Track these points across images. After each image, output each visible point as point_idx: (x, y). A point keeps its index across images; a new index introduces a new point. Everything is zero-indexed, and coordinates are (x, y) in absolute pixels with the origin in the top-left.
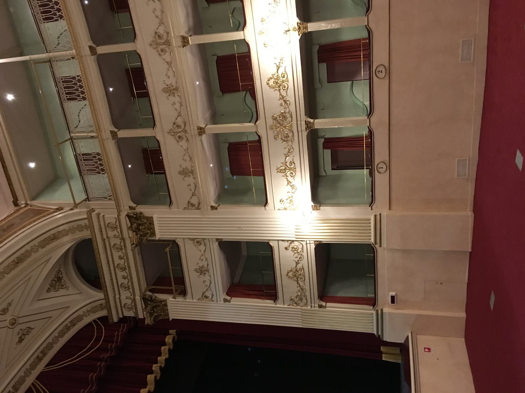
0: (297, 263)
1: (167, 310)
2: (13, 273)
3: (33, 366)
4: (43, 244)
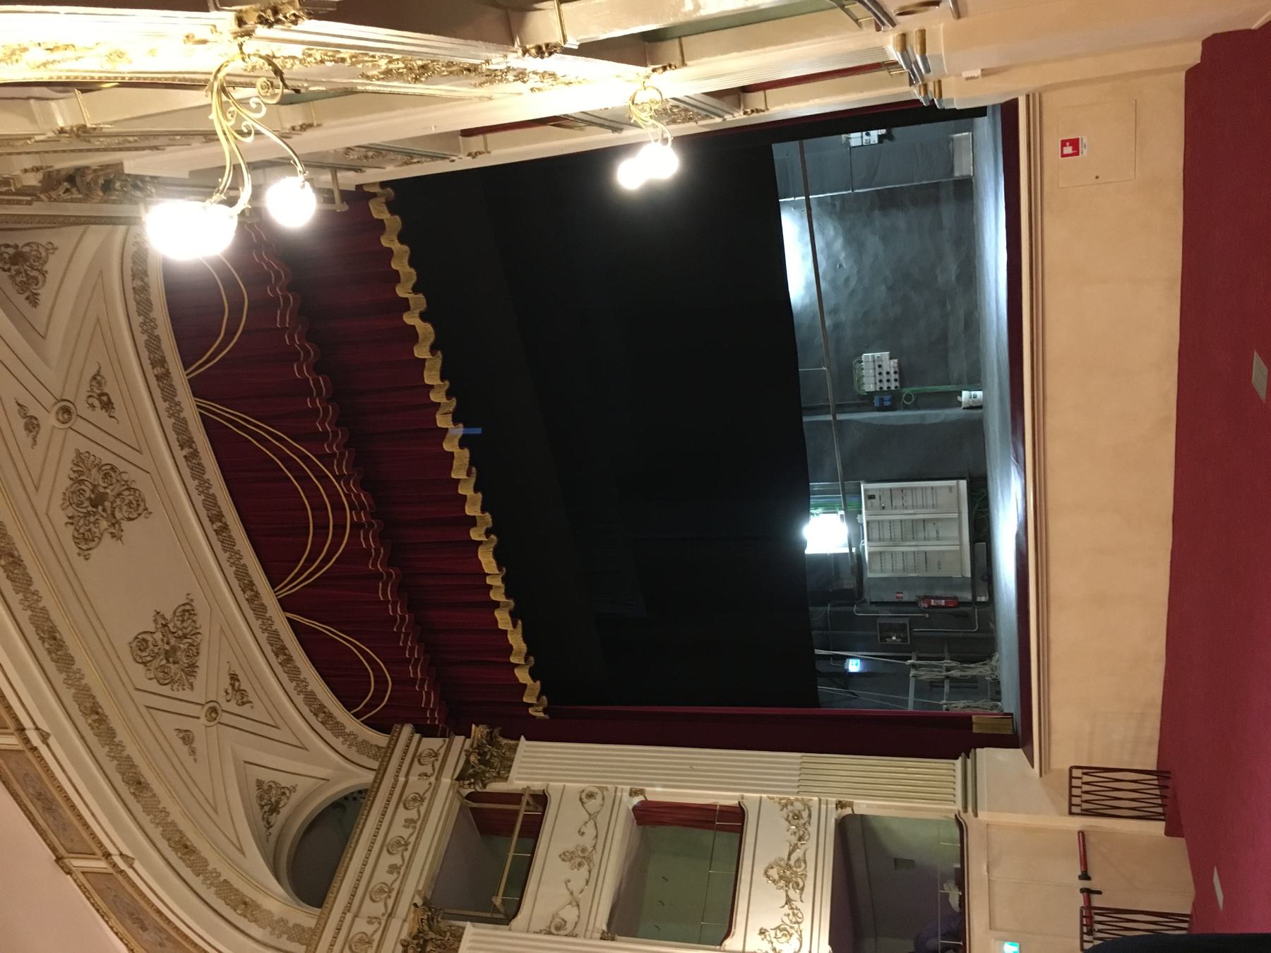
1: (512, 760)
3: (169, 393)
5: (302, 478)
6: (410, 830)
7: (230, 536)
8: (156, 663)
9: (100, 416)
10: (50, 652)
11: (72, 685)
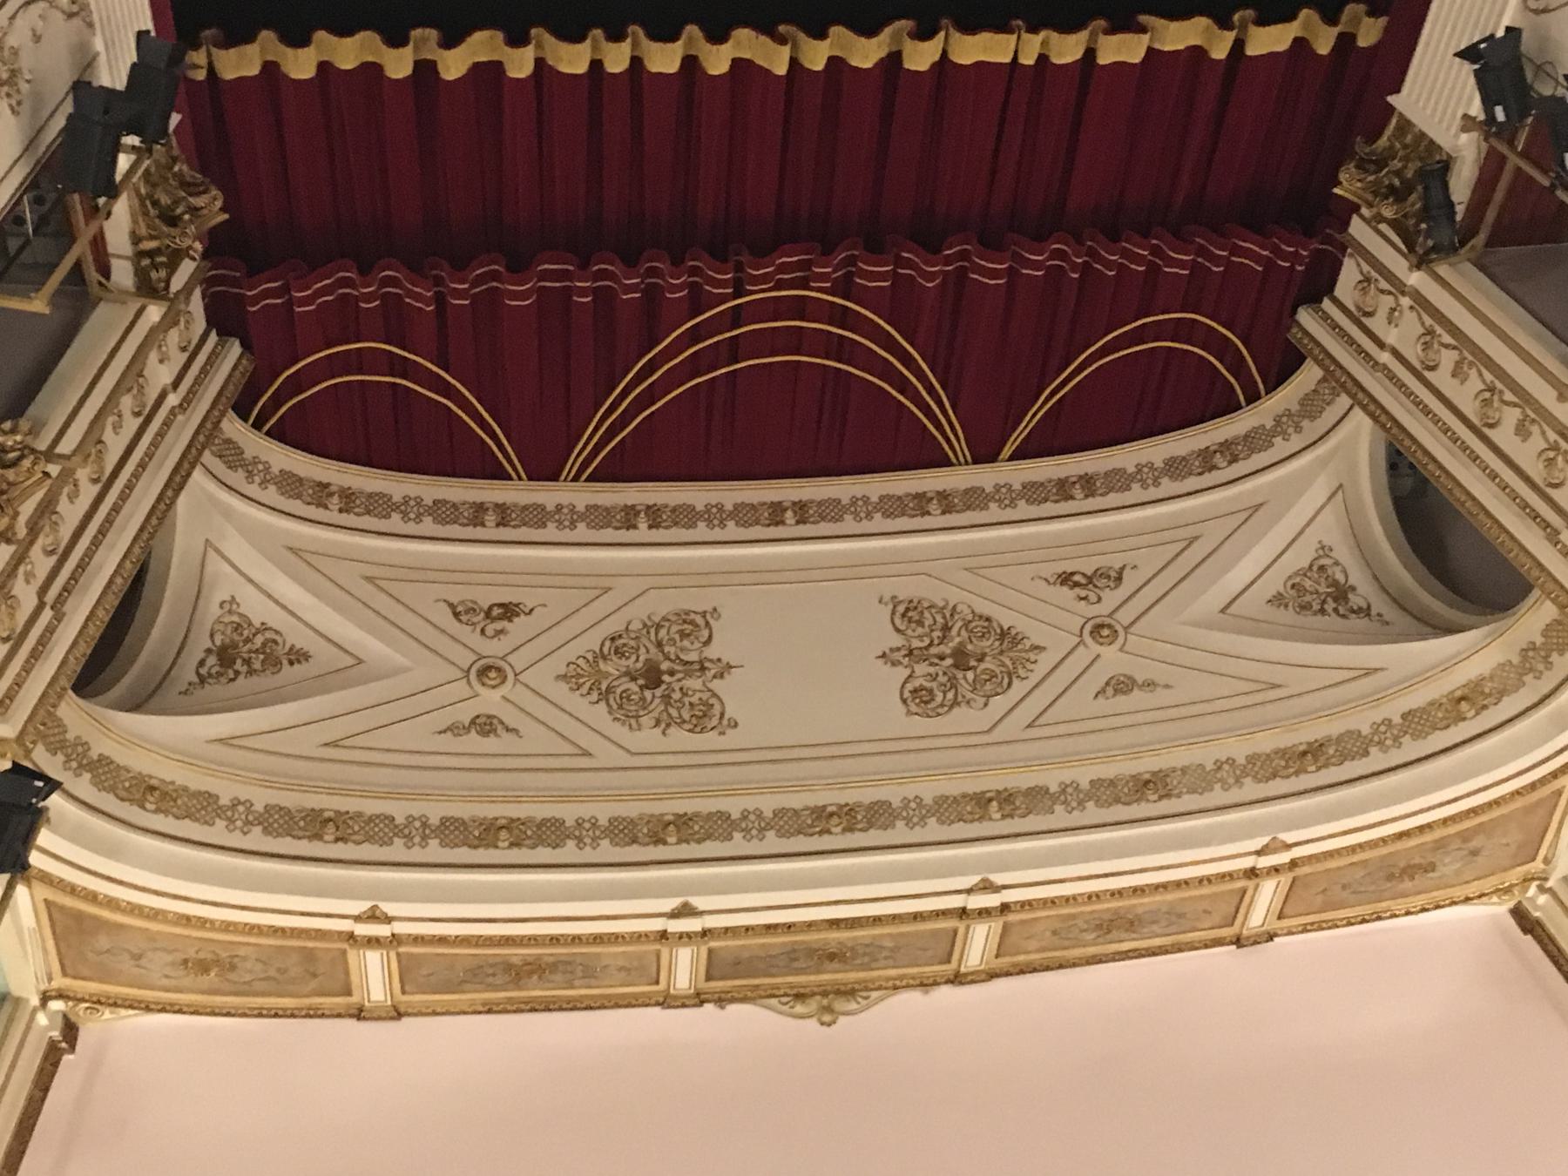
1: (1423, 135)
2: (371, 807)
4: (202, 806)
5: (734, 350)
6: (1473, 372)
7: (820, 504)
8: (965, 688)
9: (518, 628)
10: (849, 829)
11: (923, 818)
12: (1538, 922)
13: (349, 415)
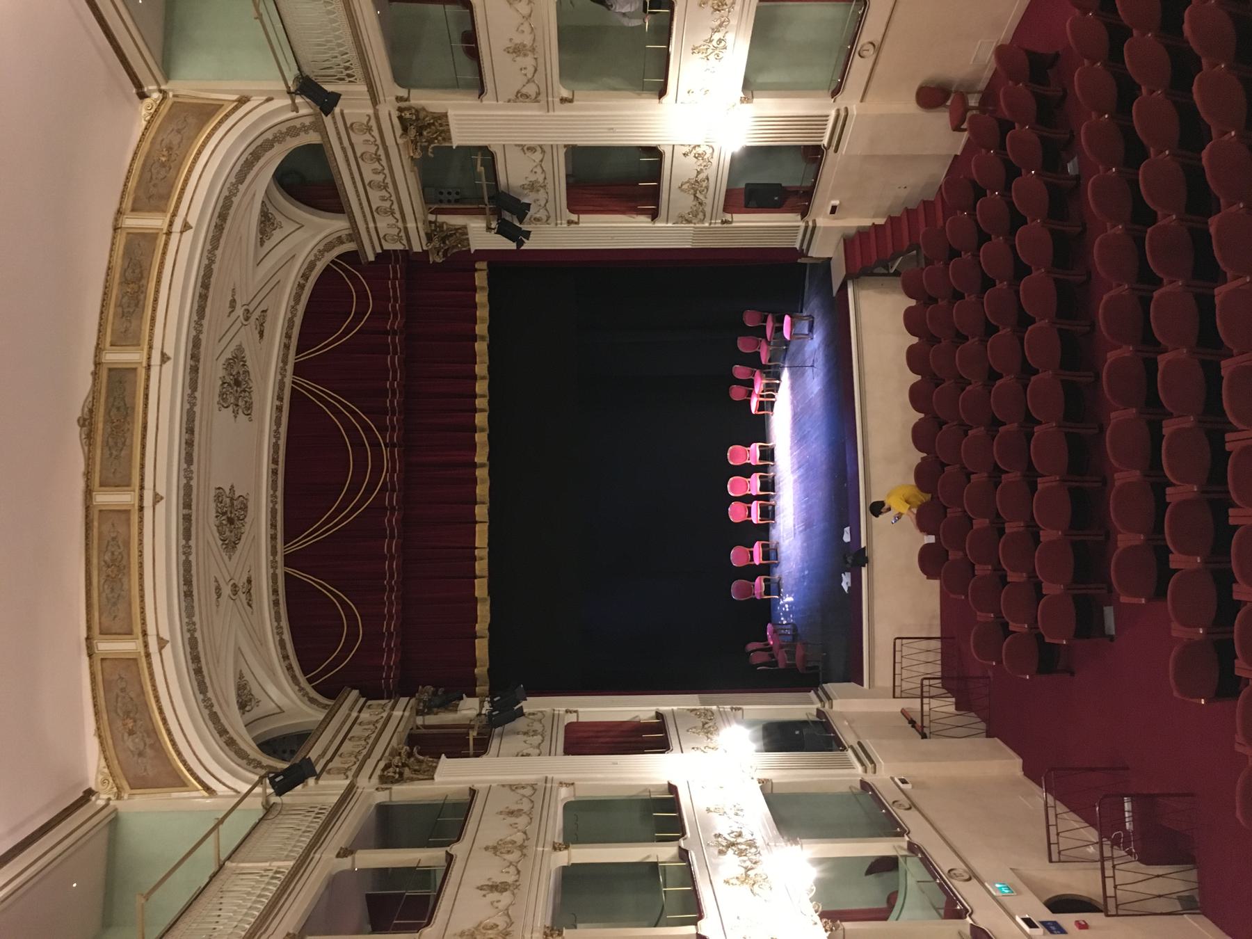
0: (699, 173)
3: (285, 362)
5: (358, 445)
12: (88, 800)
13: (334, 294)
